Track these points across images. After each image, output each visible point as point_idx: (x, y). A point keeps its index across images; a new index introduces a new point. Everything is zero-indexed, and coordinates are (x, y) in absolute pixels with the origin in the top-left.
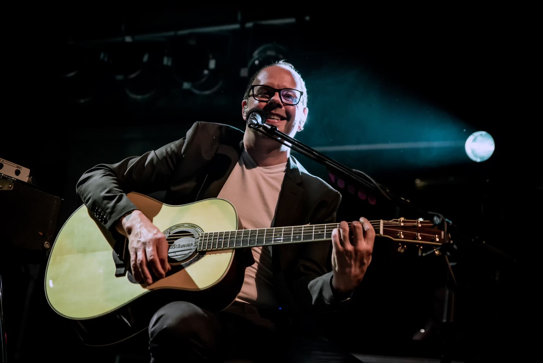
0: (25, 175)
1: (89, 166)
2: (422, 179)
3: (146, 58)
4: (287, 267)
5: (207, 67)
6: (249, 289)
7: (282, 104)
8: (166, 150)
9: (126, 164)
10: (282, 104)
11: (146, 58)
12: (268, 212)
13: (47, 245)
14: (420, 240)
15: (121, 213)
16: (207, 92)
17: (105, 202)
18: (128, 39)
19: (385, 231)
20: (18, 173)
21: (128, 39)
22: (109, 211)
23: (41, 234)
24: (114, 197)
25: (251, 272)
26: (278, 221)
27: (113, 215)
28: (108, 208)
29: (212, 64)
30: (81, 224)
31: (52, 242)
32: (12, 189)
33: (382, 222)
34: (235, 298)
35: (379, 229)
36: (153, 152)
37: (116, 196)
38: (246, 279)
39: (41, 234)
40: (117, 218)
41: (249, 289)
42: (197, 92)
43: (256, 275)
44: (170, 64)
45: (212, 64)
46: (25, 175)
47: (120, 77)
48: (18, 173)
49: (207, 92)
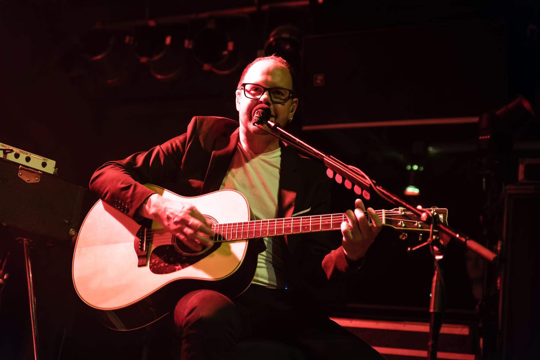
0: (51, 167)
1: (99, 164)
2: (434, 147)
3: (168, 40)
4: (294, 254)
5: (226, 48)
6: (263, 274)
7: (271, 102)
8: (172, 145)
9: (134, 158)
10: (271, 102)
11: (168, 40)
12: (273, 201)
13: (72, 232)
14: (420, 228)
15: (141, 200)
16: (226, 72)
17: (124, 192)
18: (152, 23)
19: (387, 220)
20: (44, 165)
21: (152, 23)
22: (129, 200)
23: (67, 222)
24: (129, 187)
25: (262, 258)
26: (281, 212)
27: (134, 203)
28: (127, 198)
29: (231, 46)
30: (99, 216)
31: (78, 230)
32: (39, 181)
33: (384, 211)
34: (251, 281)
35: (382, 219)
36: (158, 148)
37: (131, 185)
38: (258, 264)
39: (67, 222)
40: (138, 205)
41: (263, 274)
42: (216, 71)
43: (272, 256)
44: (190, 47)
45: (231, 46)
46: (51, 167)
47: (144, 60)
48: (44, 165)
49: (226, 72)
